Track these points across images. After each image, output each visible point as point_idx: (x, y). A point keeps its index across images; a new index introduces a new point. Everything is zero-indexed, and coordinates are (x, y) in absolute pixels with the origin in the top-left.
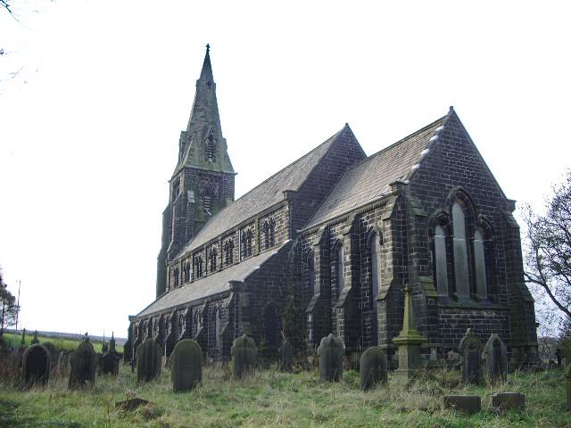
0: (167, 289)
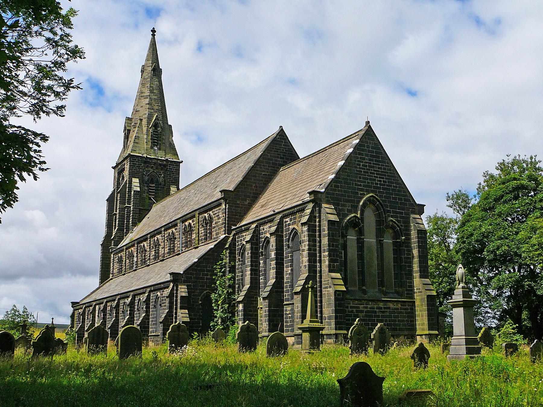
0: (111, 275)
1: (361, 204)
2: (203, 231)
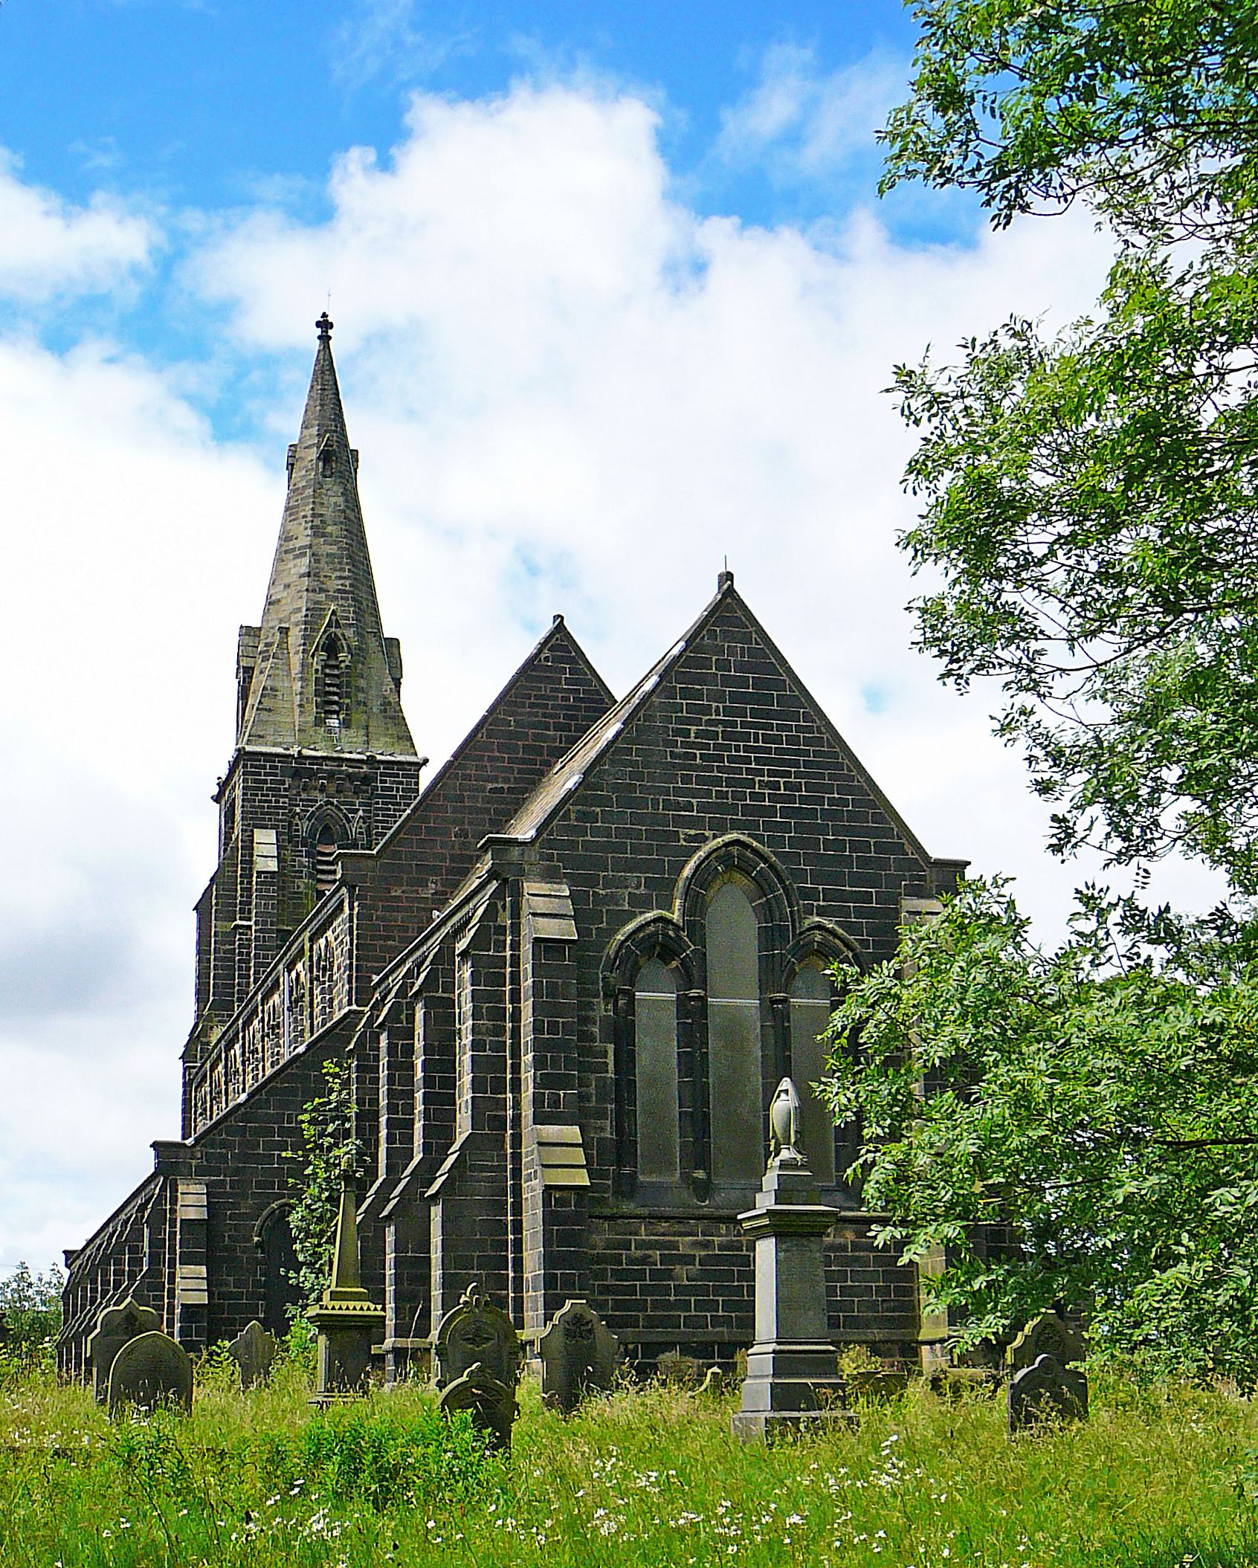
1: (687, 872)
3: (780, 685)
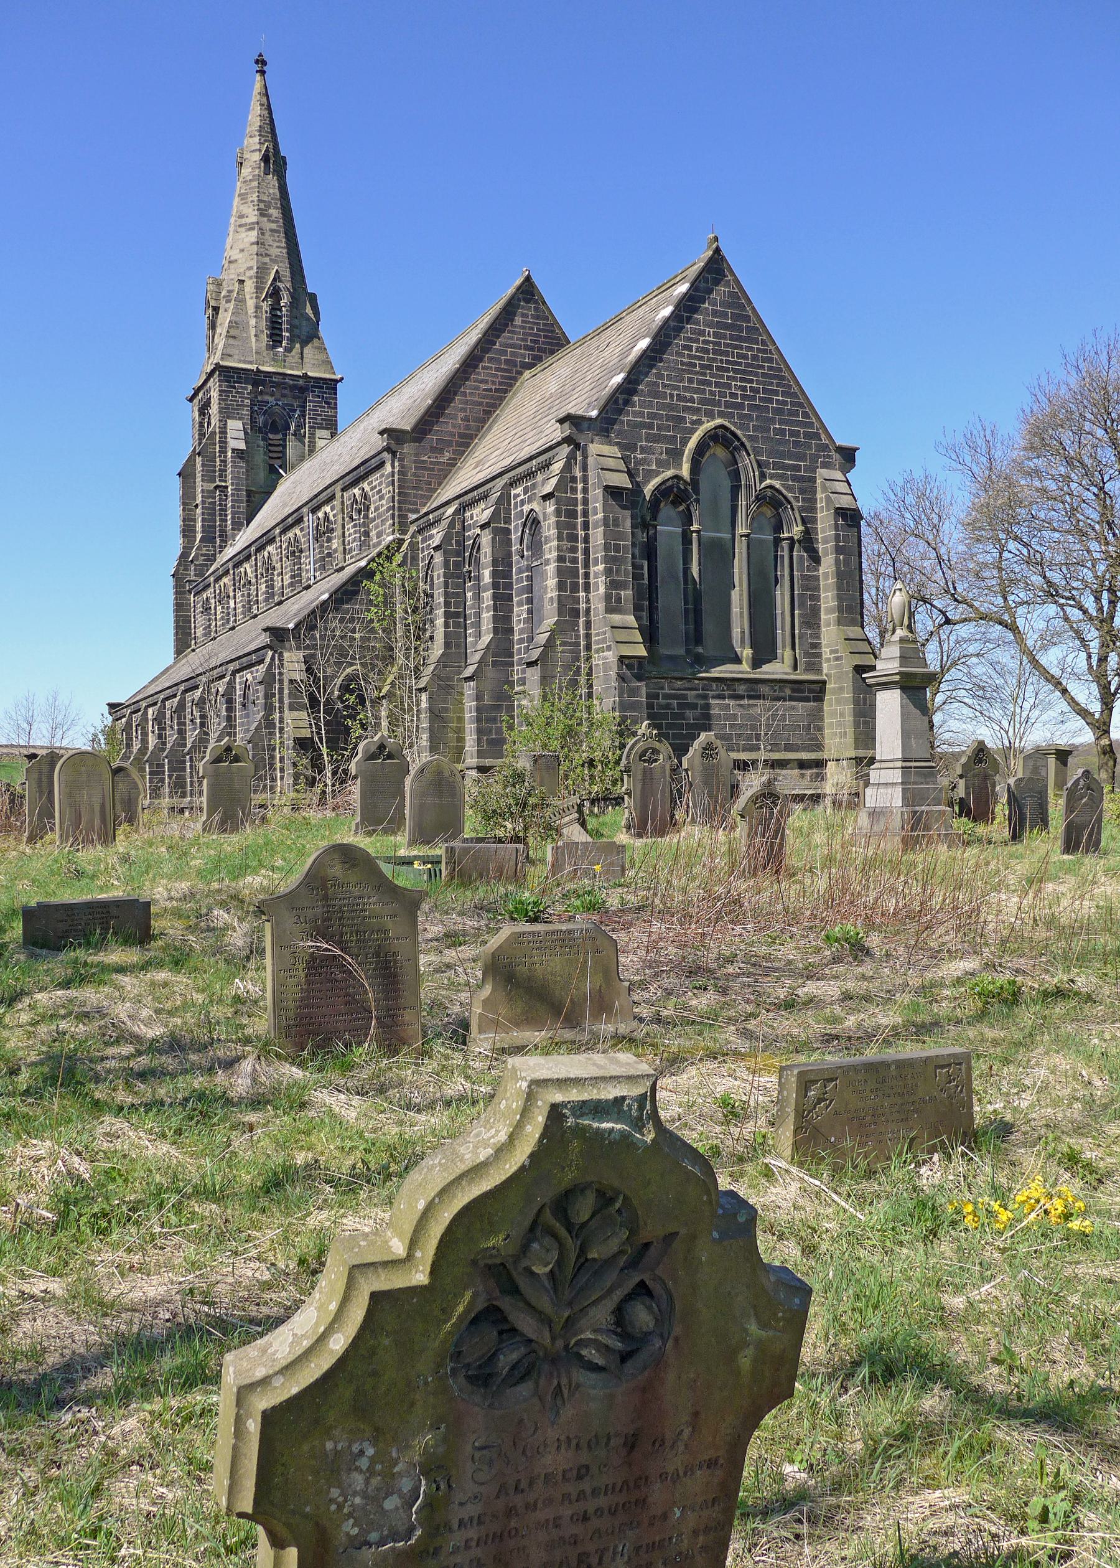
2: (352, 531)
3: (747, 319)
